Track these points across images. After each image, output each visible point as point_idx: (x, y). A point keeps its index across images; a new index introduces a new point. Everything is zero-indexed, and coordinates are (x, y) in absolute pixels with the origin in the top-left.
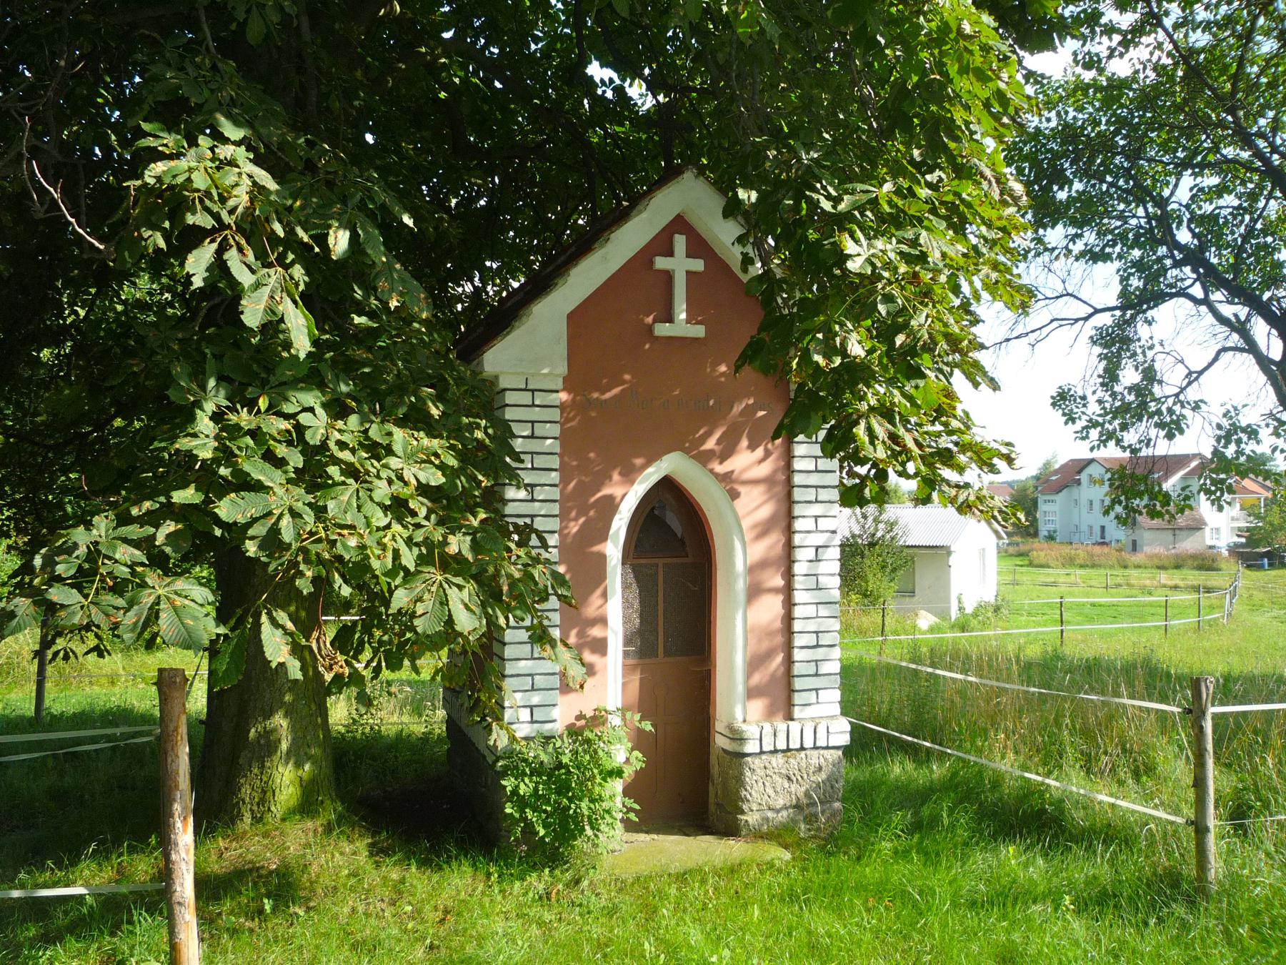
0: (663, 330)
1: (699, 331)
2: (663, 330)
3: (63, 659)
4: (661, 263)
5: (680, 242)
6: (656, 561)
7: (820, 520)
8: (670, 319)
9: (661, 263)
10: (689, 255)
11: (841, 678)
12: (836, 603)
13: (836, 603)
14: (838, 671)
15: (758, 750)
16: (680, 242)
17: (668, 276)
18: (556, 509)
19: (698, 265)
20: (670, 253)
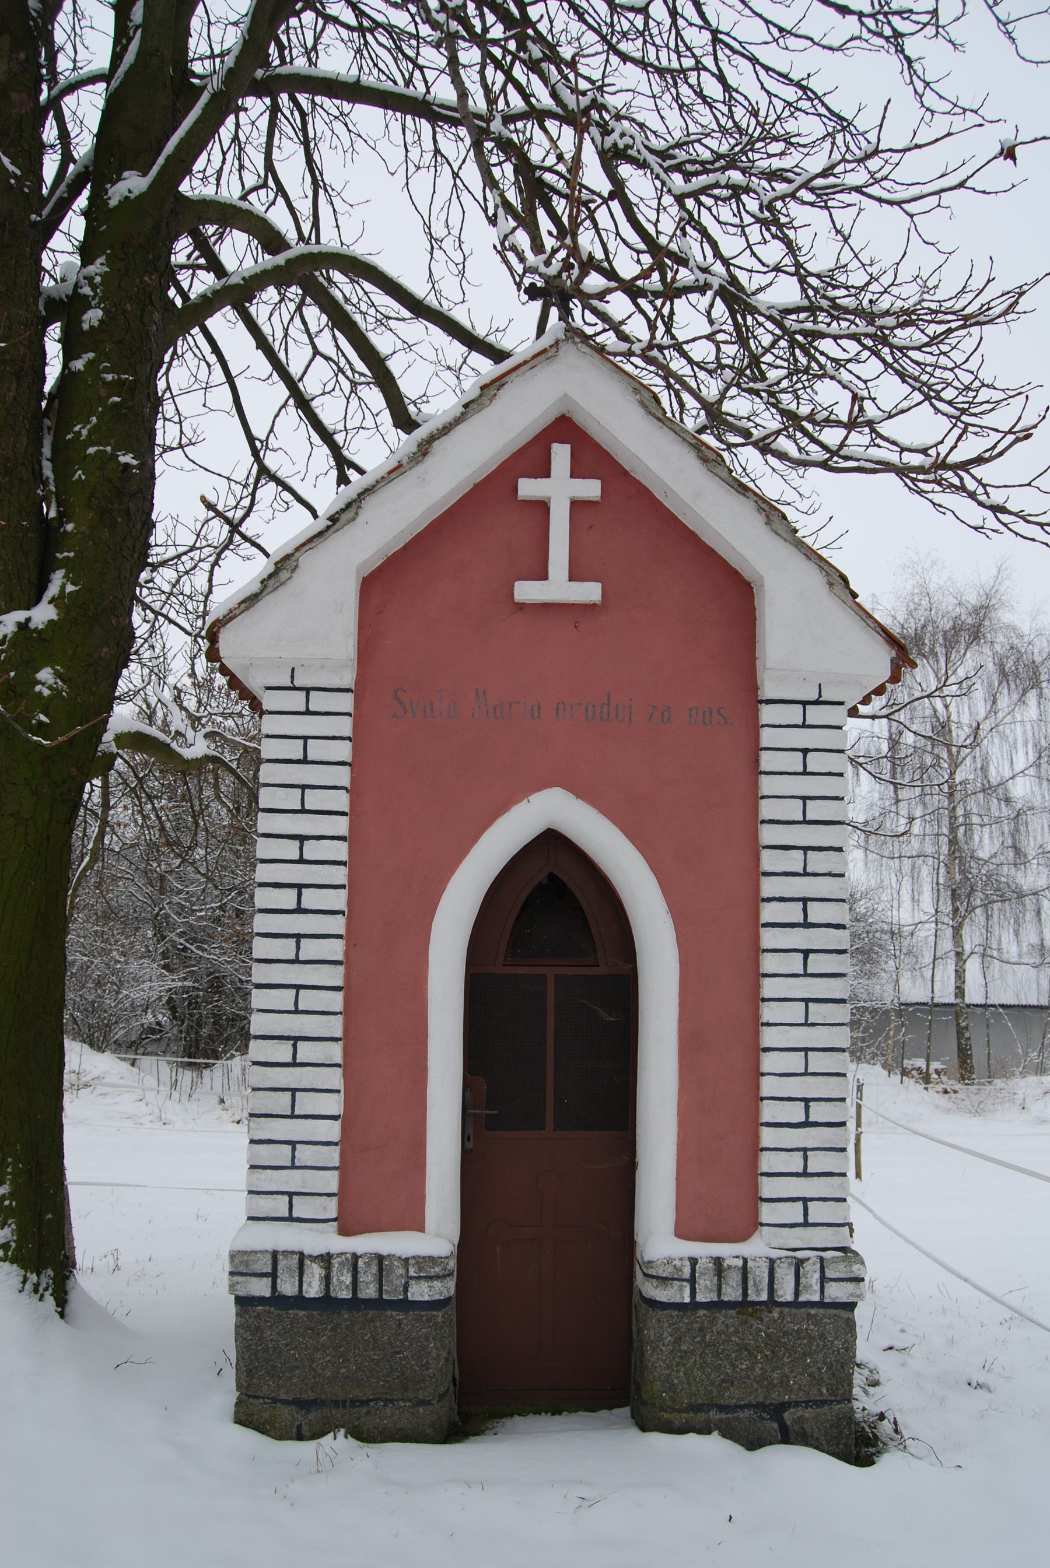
0: (527, 591)
1: (590, 592)
2: (527, 591)
3: (161, 974)
4: (528, 488)
5: (561, 454)
6: (539, 970)
7: (300, 756)
8: (542, 574)
9: (528, 488)
10: (577, 472)
11: (501, 22)
12: (843, 1050)
13: (843, 1050)
14: (495, 19)
15: (810, 755)
16: (561, 454)
17: (542, 507)
18: (340, 875)
19: (591, 489)
20: (544, 471)
